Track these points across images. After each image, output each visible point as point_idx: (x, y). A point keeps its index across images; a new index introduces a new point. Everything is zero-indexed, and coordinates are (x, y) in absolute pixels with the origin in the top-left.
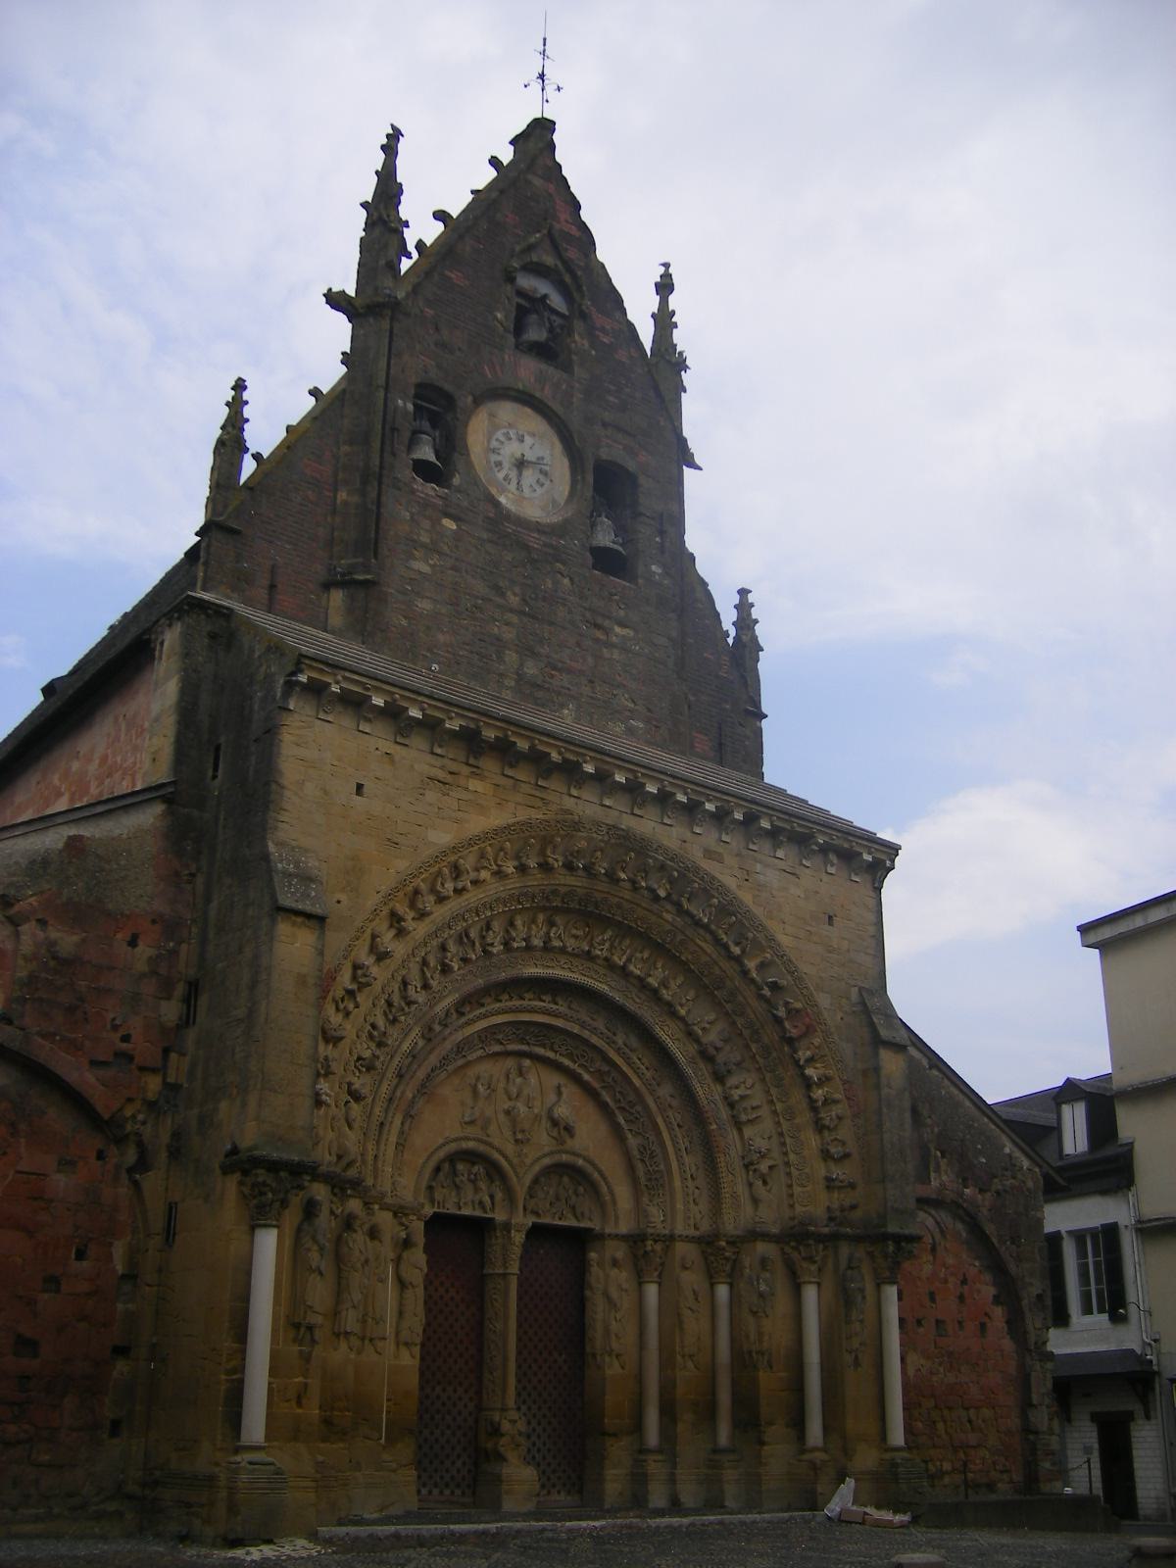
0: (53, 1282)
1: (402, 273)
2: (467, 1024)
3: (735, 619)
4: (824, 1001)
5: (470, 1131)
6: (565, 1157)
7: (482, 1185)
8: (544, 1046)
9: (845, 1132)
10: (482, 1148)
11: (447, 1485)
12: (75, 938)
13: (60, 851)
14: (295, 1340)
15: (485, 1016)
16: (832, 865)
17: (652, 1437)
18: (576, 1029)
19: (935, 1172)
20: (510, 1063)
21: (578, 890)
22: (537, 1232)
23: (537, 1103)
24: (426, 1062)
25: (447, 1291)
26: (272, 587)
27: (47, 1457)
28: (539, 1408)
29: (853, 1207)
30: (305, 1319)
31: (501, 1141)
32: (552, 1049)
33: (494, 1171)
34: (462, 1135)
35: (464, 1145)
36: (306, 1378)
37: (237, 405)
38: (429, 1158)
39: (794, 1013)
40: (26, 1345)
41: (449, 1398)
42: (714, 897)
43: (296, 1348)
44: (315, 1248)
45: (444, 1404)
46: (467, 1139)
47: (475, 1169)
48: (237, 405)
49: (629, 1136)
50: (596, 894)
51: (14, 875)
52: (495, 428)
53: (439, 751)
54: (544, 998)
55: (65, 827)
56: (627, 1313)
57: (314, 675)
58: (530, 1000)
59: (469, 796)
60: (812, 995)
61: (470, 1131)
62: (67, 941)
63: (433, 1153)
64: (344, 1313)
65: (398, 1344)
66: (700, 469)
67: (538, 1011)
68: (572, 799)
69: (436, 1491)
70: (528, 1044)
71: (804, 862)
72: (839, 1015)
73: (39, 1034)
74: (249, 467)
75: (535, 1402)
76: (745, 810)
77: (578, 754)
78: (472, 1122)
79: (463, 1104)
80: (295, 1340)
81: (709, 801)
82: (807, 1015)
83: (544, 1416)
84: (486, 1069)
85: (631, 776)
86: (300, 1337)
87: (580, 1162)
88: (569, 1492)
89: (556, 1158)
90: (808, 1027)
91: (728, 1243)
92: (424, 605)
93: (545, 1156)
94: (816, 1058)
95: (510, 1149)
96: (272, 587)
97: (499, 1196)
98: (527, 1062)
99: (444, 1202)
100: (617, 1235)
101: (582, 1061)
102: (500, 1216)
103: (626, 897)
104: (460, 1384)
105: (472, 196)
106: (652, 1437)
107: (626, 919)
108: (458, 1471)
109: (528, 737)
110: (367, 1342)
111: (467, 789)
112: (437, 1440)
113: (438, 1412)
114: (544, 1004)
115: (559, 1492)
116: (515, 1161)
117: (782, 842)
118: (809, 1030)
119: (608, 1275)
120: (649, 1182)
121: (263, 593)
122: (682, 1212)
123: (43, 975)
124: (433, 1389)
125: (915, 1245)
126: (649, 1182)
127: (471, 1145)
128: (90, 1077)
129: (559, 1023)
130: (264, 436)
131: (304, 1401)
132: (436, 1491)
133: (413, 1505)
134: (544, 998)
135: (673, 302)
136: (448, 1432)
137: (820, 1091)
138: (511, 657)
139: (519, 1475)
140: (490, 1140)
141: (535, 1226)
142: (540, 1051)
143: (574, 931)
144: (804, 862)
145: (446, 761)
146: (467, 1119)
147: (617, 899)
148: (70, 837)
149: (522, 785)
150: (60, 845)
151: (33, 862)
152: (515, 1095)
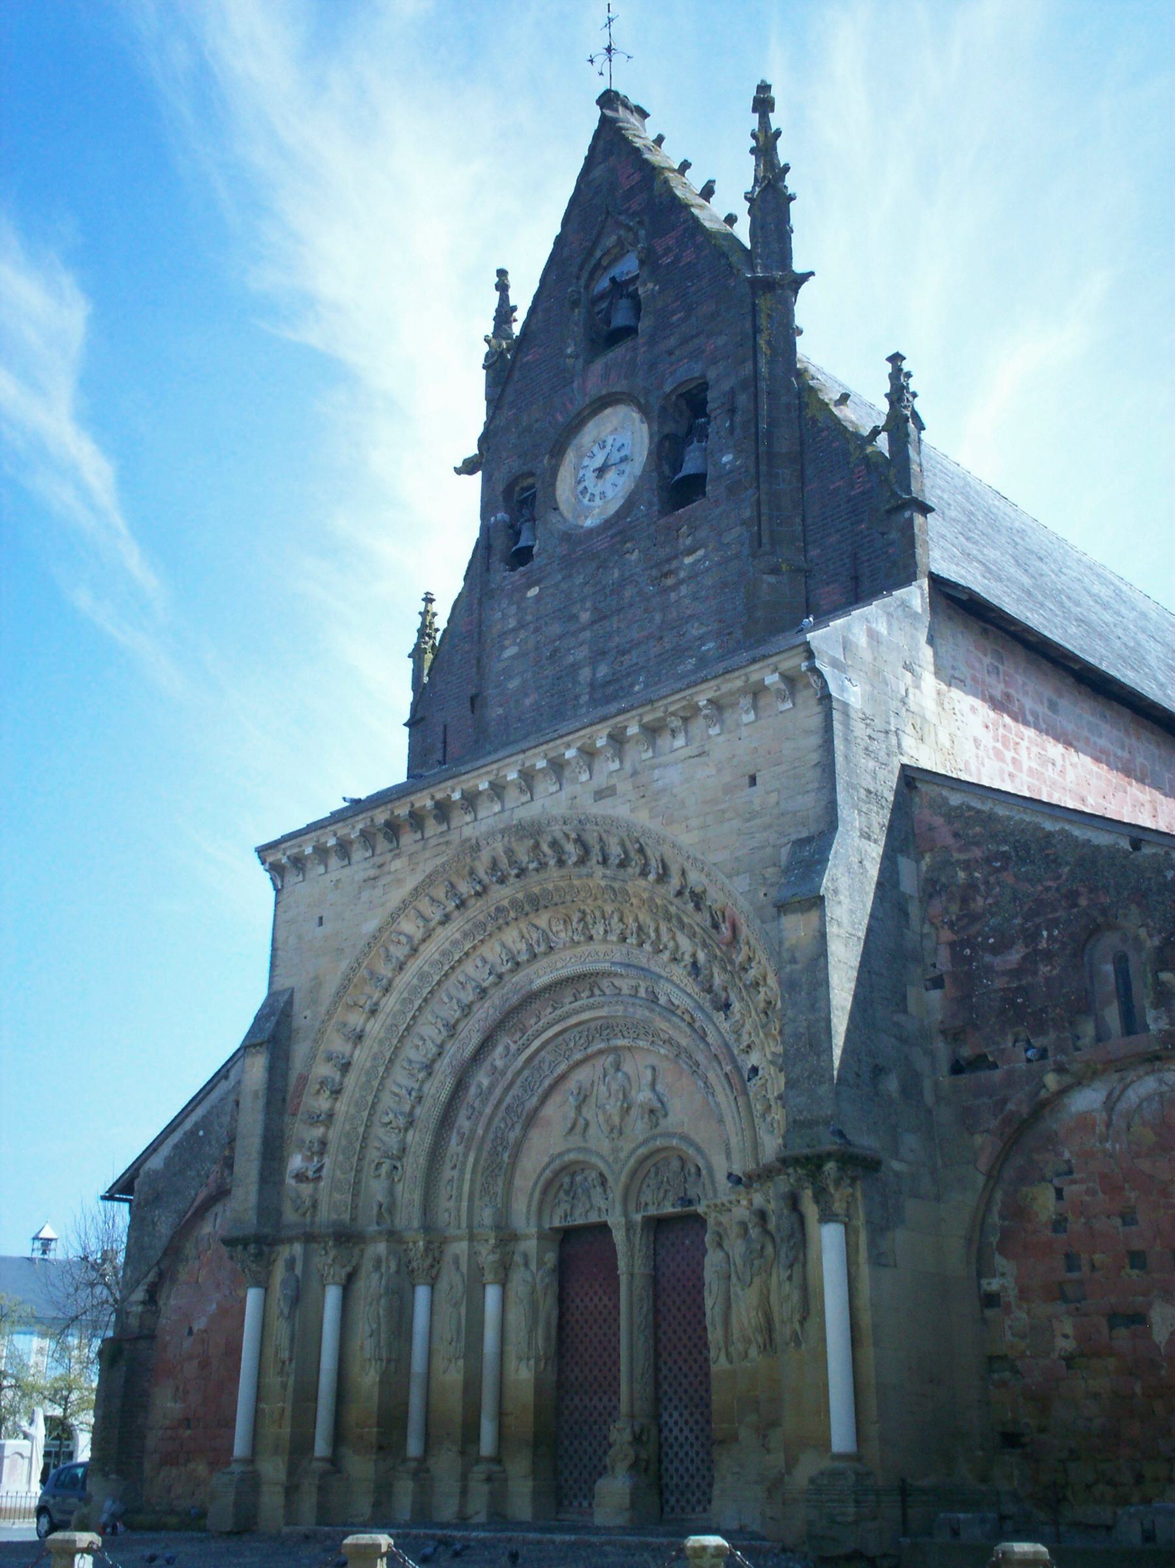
1: (748, 245)
3: (888, 391)
19: (1156, 1006)
28: (692, 1414)
41: (605, 1408)
45: (600, 1415)
52: (580, 457)
66: (812, 274)
72: (764, 890)
75: (676, 1408)
92: (513, 684)
93: (638, 1147)
105: (512, 304)
113: (595, 1422)
116: (611, 1159)
135: (776, 120)
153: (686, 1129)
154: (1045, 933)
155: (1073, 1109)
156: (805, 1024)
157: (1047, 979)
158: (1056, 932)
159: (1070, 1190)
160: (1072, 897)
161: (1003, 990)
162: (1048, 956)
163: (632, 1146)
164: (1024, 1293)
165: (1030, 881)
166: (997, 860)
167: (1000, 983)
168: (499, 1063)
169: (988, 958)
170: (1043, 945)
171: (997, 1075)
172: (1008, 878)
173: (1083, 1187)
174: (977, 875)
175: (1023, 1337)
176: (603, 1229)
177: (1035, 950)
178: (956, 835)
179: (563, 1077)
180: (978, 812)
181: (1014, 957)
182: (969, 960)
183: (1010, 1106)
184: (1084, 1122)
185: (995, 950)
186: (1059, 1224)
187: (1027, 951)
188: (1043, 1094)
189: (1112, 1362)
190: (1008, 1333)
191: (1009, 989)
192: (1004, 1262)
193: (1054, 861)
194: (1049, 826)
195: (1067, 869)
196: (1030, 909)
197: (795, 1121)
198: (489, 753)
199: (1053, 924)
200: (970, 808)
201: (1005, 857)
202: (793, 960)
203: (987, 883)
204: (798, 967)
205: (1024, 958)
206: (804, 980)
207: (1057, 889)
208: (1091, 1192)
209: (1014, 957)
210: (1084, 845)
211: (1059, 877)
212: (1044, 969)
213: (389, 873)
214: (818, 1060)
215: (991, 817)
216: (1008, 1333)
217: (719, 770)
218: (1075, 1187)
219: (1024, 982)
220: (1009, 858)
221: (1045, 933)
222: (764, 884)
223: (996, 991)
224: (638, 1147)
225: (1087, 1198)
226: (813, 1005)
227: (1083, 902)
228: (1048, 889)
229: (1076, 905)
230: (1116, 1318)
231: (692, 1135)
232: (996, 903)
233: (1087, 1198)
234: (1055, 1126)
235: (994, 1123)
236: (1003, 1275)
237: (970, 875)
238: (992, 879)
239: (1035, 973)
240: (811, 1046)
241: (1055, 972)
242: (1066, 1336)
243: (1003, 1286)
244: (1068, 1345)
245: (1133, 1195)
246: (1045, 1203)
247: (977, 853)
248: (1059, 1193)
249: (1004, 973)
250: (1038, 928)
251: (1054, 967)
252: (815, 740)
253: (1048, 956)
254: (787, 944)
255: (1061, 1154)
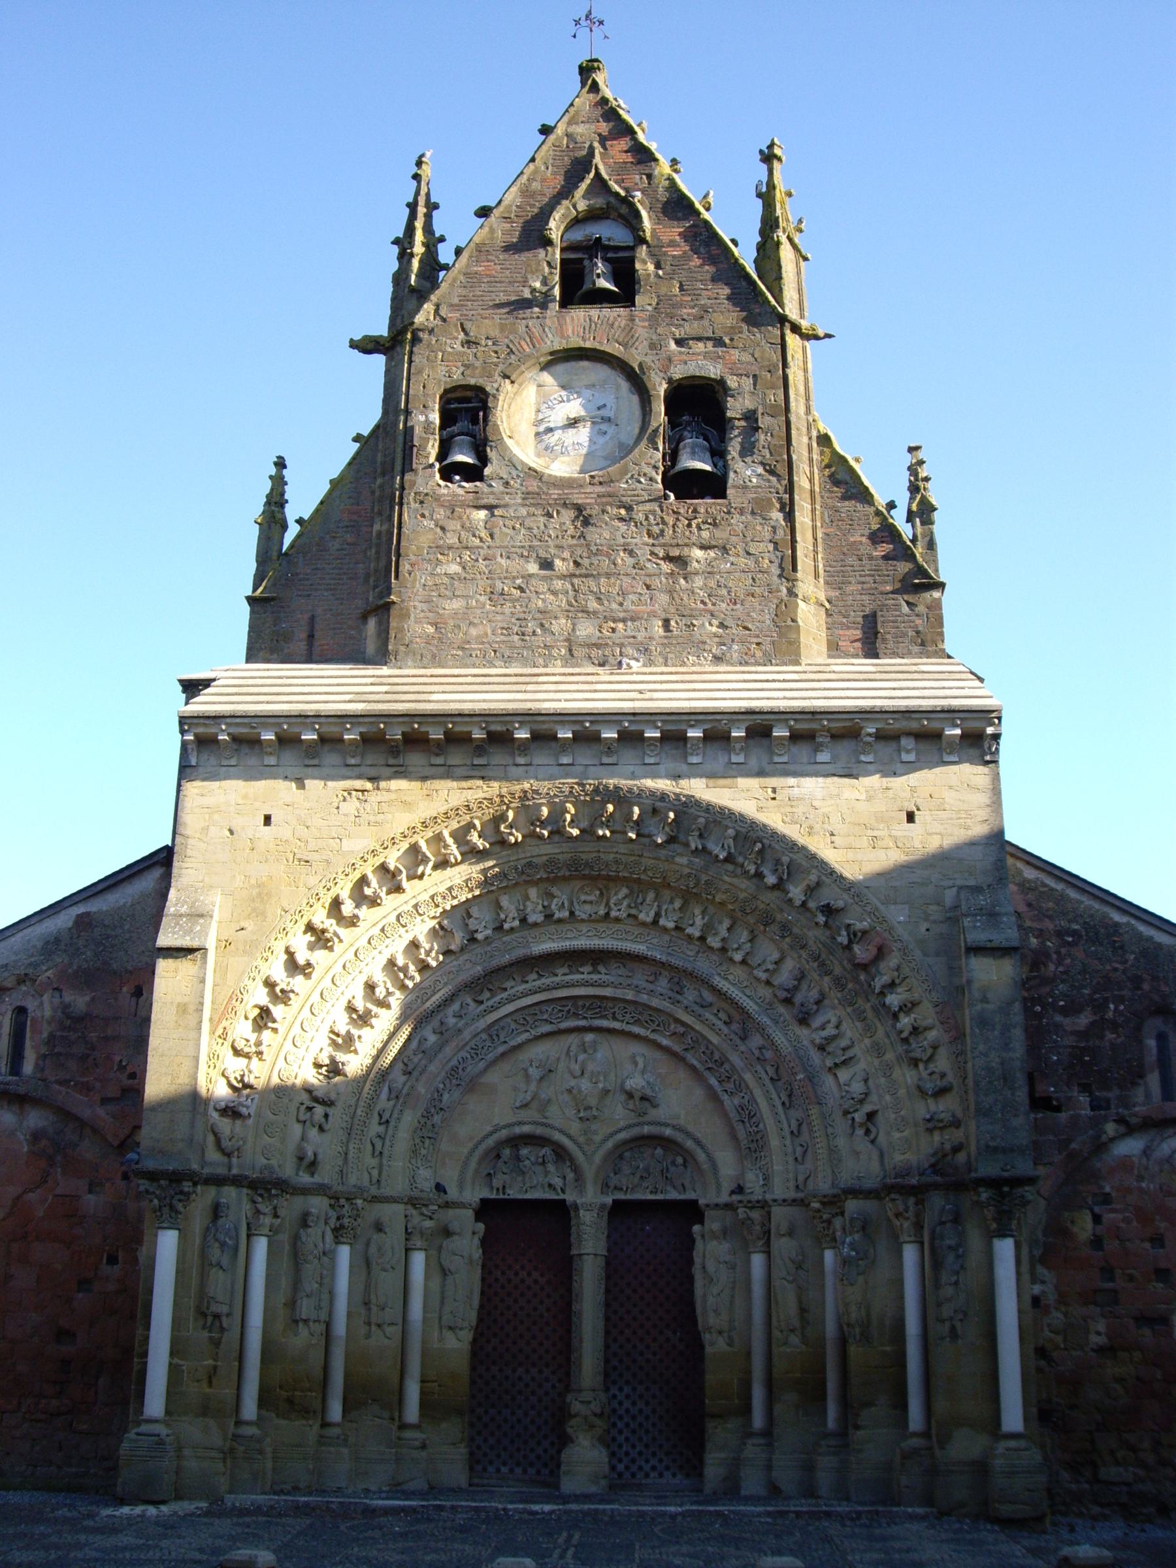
0: (84, 1284)
2: (487, 1012)
4: (898, 916)
5: (524, 1115)
6: (646, 1130)
7: (551, 1167)
8: (605, 1017)
9: (943, 1062)
10: (539, 1131)
11: (531, 1464)
12: (87, 998)
13: (70, 929)
14: (204, 1327)
15: (510, 1000)
16: (908, 752)
17: (758, 1420)
18: (630, 995)
20: (573, 1040)
21: (560, 857)
22: (620, 1211)
23: (612, 1075)
24: (440, 1056)
25: (529, 1274)
26: (311, 636)
27: (85, 1427)
29: (957, 1149)
30: (208, 1308)
31: (562, 1120)
32: (615, 1018)
33: (561, 1154)
34: (514, 1120)
35: (518, 1130)
36: (214, 1360)
37: (279, 482)
38: (476, 1147)
39: (856, 936)
40: (63, 1335)
41: (533, 1379)
42: (727, 827)
43: (206, 1334)
44: (217, 1245)
46: (520, 1123)
47: (543, 1151)
48: (279, 482)
49: (725, 1097)
50: (583, 856)
51: (32, 956)
53: (353, 761)
54: (581, 970)
55: (74, 908)
56: (734, 1288)
57: (200, 730)
58: (564, 975)
59: (393, 796)
60: (877, 909)
61: (524, 1115)
62: (79, 1001)
63: (480, 1143)
64: (299, 1302)
65: (441, 1328)
67: (579, 983)
68: (521, 768)
69: (519, 1470)
70: (585, 1018)
71: (863, 758)
72: (925, 925)
73: (57, 1082)
74: (293, 531)
76: (747, 724)
77: (505, 723)
78: (525, 1106)
79: (515, 1089)
80: (204, 1327)
81: (692, 726)
82: (877, 933)
83: (654, 1396)
84: (540, 1051)
85: (577, 728)
86: (209, 1324)
87: (668, 1132)
88: (688, 1475)
89: (636, 1131)
90: (880, 949)
91: (823, 1203)
94: (897, 981)
95: (575, 1128)
96: (311, 636)
97: (571, 1176)
98: (589, 1037)
99: (504, 1187)
100: (717, 1205)
101: (654, 1026)
102: (569, 1197)
103: (622, 851)
104: (547, 1365)
106: (758, 1420)
107: (633, 873)
108: (545, 1451)
109: (439, 723)
110: (374, 1328)
111: (388, 790)
112: (519, 1421)
114: (582, 976)
115: (674, 1475)
116: (581, 1139)
117: (821, 744)
118: (881, 953)
119: (711, 1252)
120: (753, 1148)
121: (302, 646)
122: (779, 1177)
123: (58, 1034)
124: (514, 1371)
125: (1027, 1188)
126: (753, 1148)
127: (526, 1129)
128: (101, 1112)
129: (607, 992)
130: (302, 502)
131: (214, 1381)
132: (519, 1470)
133: (463, 1481)
134: (581, 970)
136: (532, 1413)
137: (906, 1020)
138: (560, 625)
139: (586, 1457)
140: (550, 1121)
141: (616, 1202)
142: (605, 1023)
143: (583, 898)
144: (863, 758)
145: (363, 769)
146: (518, 1104)
147: (612, 856)
148: (78, 916)
149: (455, 769)
150: (70, 924)
151: (47, 943)
152: (579, 1073)
153: (682, 1122)
154: (1112, 1006)
155: (1116, 1152)
156: (997, 1060)
157: (1112, 1044)
158: (1122, 1007)
159: (1108, 1217)
160: (1136, 981)
161: (1072, 1047)
162: (1114, 1026)
163: (610, 1130)
164: (1062, 1299)
165: (1100, 959)
166: (1069, 935)
167: (1070, 1041)
168: (451, 1021)
169: (1058, 1018)
170: (1110, 1015)
171: (1063, 1116)
172: (1078, 952)
173: (1120, 1216)
174: (1049, 944)
175: (1056, 1333)
176: (558, 1213)
177: (1102, 1018)
178: (1029, 905)
179: (519, 1047)
180: (1052, 889)
181: (1084, 1020)
182: (1039, 1016)
183: (1073, 1146)
184: (1125, 1164)
185: (1064, 1011)
186: (1097, 1242)
187: (1095, 1018)
188: (1104, 1138)
189: (1137, 1355)
190: (1046, 1329)
191: (1077, 1047)
192: (1045, 1272)
193: (1122, 947)
194: (1117, 917)
195: (1132, 957)
196: (1098, 983)
197: (988, 1146)
198: (409, 667)
199: (1119, 1000)
200: (1045, 885)
201: (1074, 933)
202: (985, 1000)
203: (1058, 953)
204: (990, 1007)
205: (1093, 1024)
206: (997, 1020)
207: (1124, 972)
208: (1127, 1220)
209: (1084, 1020)
210: (1147, 940)
211: (1126, 962)
212: (1110, 1036)
213: (388, 790)
214: (1013, 1094)
215: (1061, 898)
216: (1046, 1329)
217: (870, 799)
218: (1112, 1215)
219: (1091, 1043)
220: (1080, 936)
221: (1112, 1006)
222: (926, 920)
223: (1065, 1047)
224: (620, 1130)
225: (1123, 1225)
226: (1007, 1044)
227: (1146, 987)
228: (1116, 969)
229: (1139, 988)
230: (1143, 1320)
231: (690, 1128)
232: (1065, 972)
233: (1123, 1225)
234: (1098, 1165)
235: (1057, 1158)
236: (1043, 1282)
237: (1043, 943)
238: (1063, 951)
239: (1102, 1038)
240: (1005, 1079)
241: (1119, 1040)
242: (1098, 1333)
243: (1043, 1292)
244: (1101, 1340)
245: (1163, 1225)
246: (1084, 1227)
247: (1049, 925)
248: (1097, 1219)
249: (1074, 1033)
250: (1106, 1001)
251: (1119, 1036)
252: (984, 798)
253: (1114, 1026)
254: (976, 985)
255: (1103, 1188)
